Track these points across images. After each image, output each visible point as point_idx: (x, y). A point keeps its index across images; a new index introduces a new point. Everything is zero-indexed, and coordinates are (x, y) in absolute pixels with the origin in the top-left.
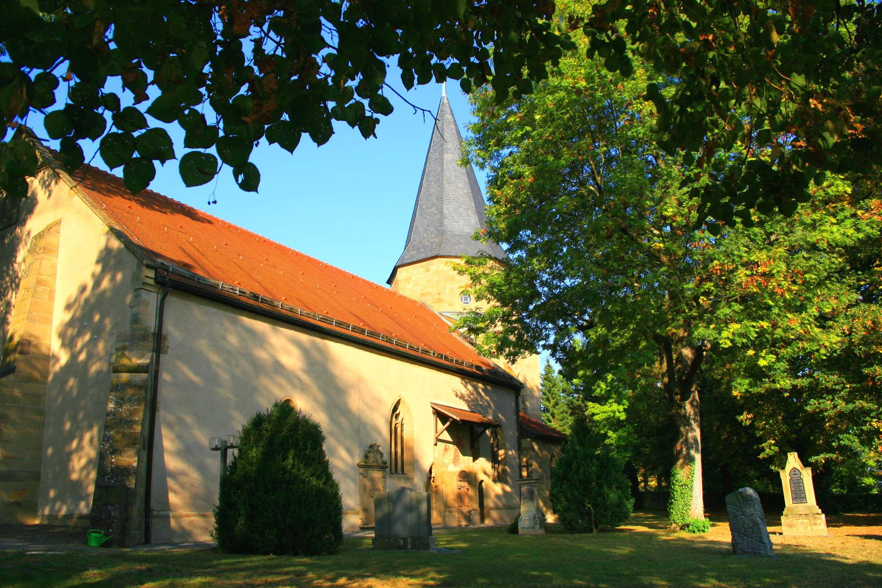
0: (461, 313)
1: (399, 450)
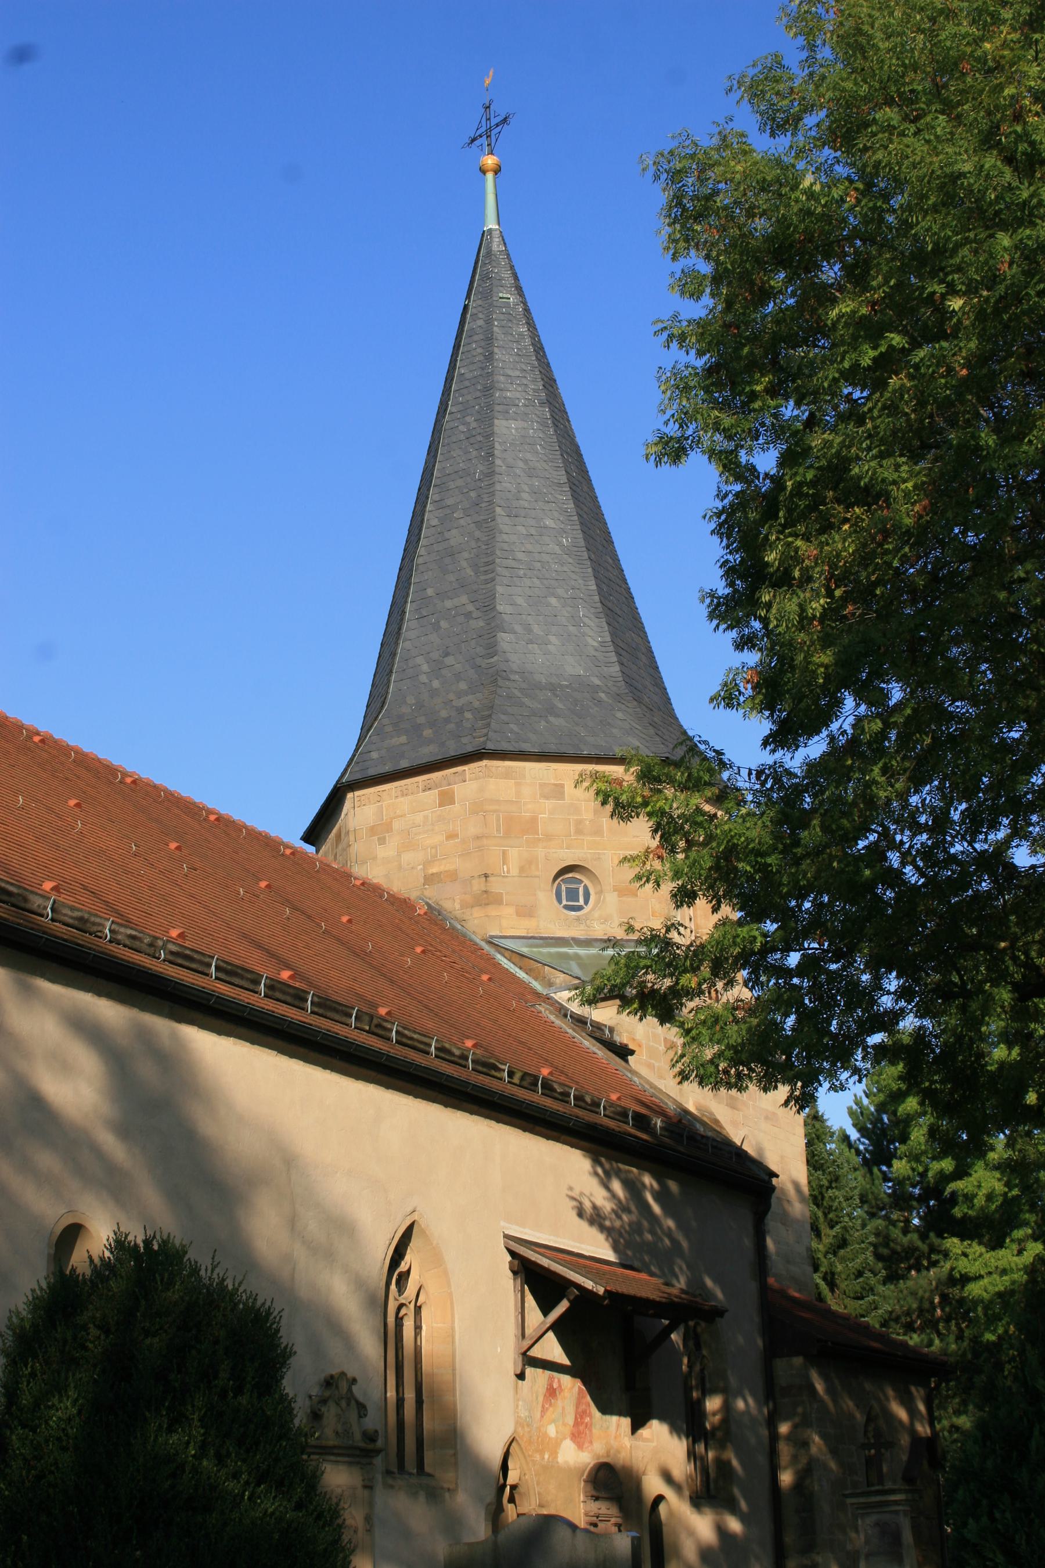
0: (611, 942)
1: (410, 1395)
